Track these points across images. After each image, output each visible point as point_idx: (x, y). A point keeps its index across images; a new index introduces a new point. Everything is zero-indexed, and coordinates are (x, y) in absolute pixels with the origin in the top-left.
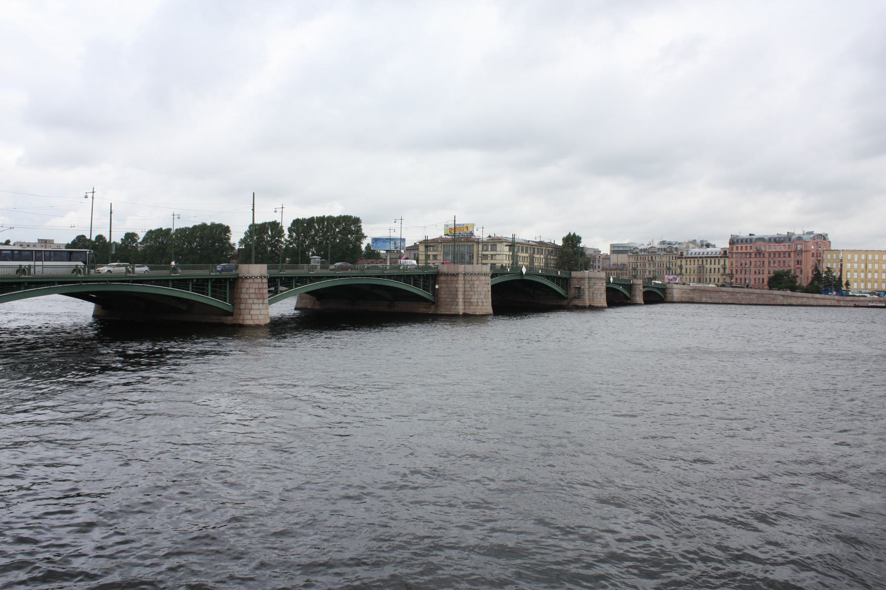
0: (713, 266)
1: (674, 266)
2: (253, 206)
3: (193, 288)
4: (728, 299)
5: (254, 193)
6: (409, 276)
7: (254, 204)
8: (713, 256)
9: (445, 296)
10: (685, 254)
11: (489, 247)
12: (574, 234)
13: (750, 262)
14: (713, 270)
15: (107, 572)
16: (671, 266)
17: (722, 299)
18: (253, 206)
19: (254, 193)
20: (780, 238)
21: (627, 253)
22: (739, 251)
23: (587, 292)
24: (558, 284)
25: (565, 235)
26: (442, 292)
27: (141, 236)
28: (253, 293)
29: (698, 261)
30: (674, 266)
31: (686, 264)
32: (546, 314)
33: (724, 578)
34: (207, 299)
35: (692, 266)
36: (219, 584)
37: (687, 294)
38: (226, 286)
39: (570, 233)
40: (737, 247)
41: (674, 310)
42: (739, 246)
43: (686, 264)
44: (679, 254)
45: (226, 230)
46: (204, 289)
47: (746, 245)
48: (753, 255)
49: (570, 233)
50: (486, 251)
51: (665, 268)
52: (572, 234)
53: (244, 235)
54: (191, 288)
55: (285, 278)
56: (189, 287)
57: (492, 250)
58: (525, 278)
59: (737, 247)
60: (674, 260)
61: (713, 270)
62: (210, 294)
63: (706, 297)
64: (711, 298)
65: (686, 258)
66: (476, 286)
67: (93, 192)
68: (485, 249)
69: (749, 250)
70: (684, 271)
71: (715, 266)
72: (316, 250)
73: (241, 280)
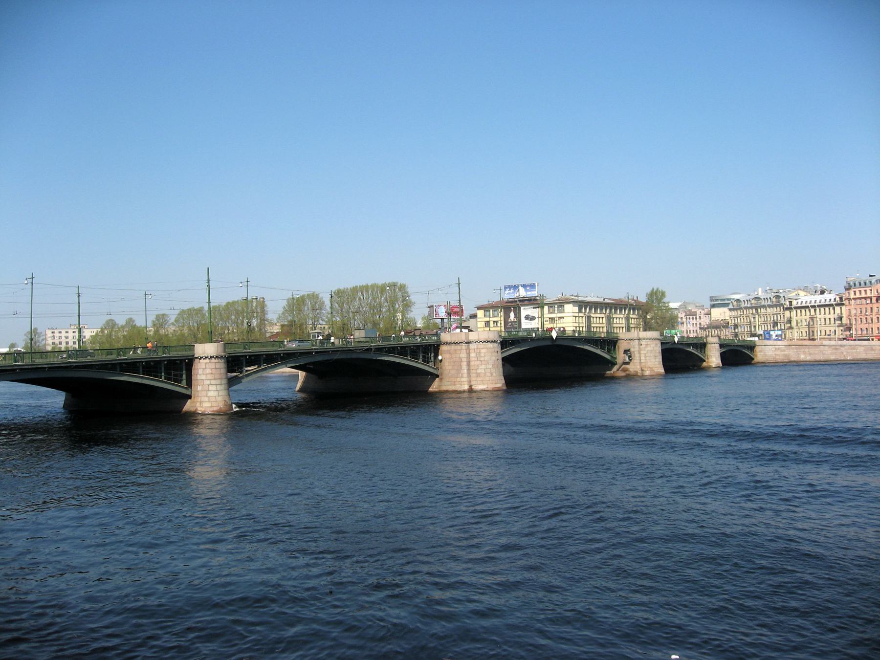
2: (209, 282)
3: (143, 371)
4: (831, 354)
5: (208, 269)
6: (597, 340)
7: (209, 280)
9: (203, 377)
10: (794, 303)
11: (556, 309)
12: (657, 289)
13: (872, 308)
14: (828, 320)
17: (824, 354)
18: (209, 282)
19: (208, 269)
20: (407, 311)
21: (728, 306)
22: (858, 295)
23: (637, 355)
24: (602, 348)
25: (649, 291)
26: (446, 364)
27: (173, 317)
29: (810, 311)
33: (232, 605)
34: (691, 349)
35: (803, 317)
37: (782, 351)
38: (182, 367)
39: (653, 289)
40: (855, 292)
42: (857, 290)
45: (262, 303)
46: (157, 372)
47: (860, 289)
48: (874, 300)
49: (653, 289)
50: (551, 313)
52: (655, 290)
53: (124, 323)
54: (141, 371)
55: (284, 354)
56: (139, 370)
57: (559, 312)
58: (557, 343)
59: (855, 292)
61: (828, 320)
62: (163, 377)
63: (804, 353)
64: (810, 354)
65: (796, 308)
66: (482, 355)
67: (32, 278)
68: (551, 311)
69: (869, 295)
70: (794, 324)
72: (336, 321)
73: (619, 341)
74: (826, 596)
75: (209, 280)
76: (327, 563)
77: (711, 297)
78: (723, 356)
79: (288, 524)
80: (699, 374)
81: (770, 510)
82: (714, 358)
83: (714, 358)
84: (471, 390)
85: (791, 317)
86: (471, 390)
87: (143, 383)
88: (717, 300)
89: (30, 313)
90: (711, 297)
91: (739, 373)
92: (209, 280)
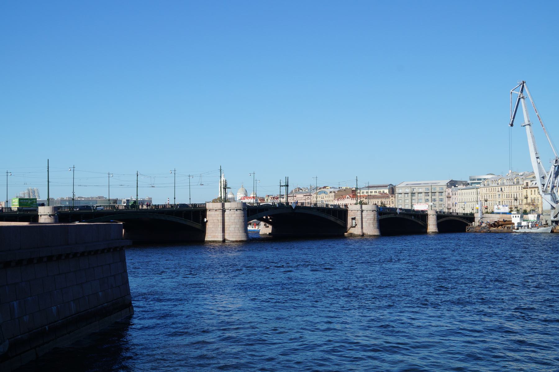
0: (308, 201)
1: (490, 198)
2: (48, 168)
5: (48, 160)
8: (533, 186)
15: (288, 353)
16: (488, 198)
18: (48, 168)
19: (48, 160)
28: (215, 220)
30: (490, 198)
31: (532, 194)
32: (319, 243)
34: (332, 218)
36: (477, 342)
41: (381, 246)
43: (532, 194)
44: (525, 184)
51: (513, 198)
60: (520, 191)
67: (74, 168)
71: (330, 199)
74: (237, 350)
75: (48, 167)
76: (207, 290)
77: (470, 177)
78: (439, 225)
79: (541, 273)
80: (422, 237)
81: (512, 309)
82: (432, 226)
83: (432, 226)
84: (363, 235)
85: (527, 195)
86: (363, 235)
87: (444, 220)
88: (474, 180)
89: (281, 190)
90: (470, 177)
91: (452, 239)
92: (48, 167)
